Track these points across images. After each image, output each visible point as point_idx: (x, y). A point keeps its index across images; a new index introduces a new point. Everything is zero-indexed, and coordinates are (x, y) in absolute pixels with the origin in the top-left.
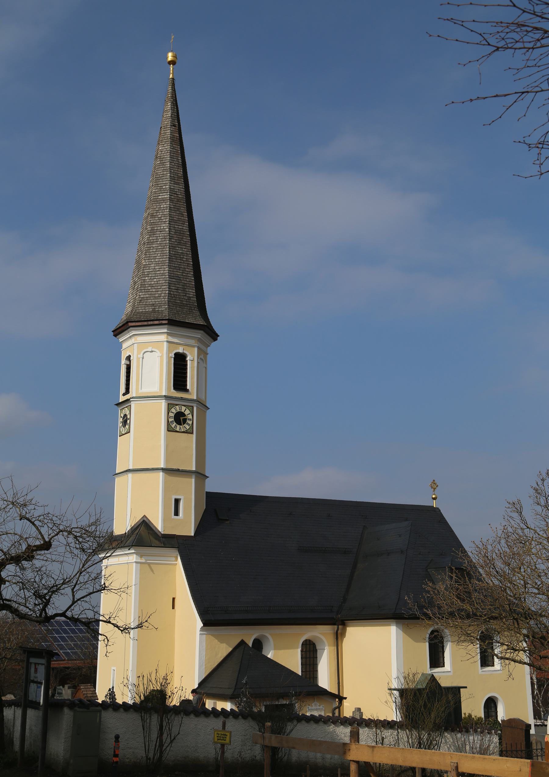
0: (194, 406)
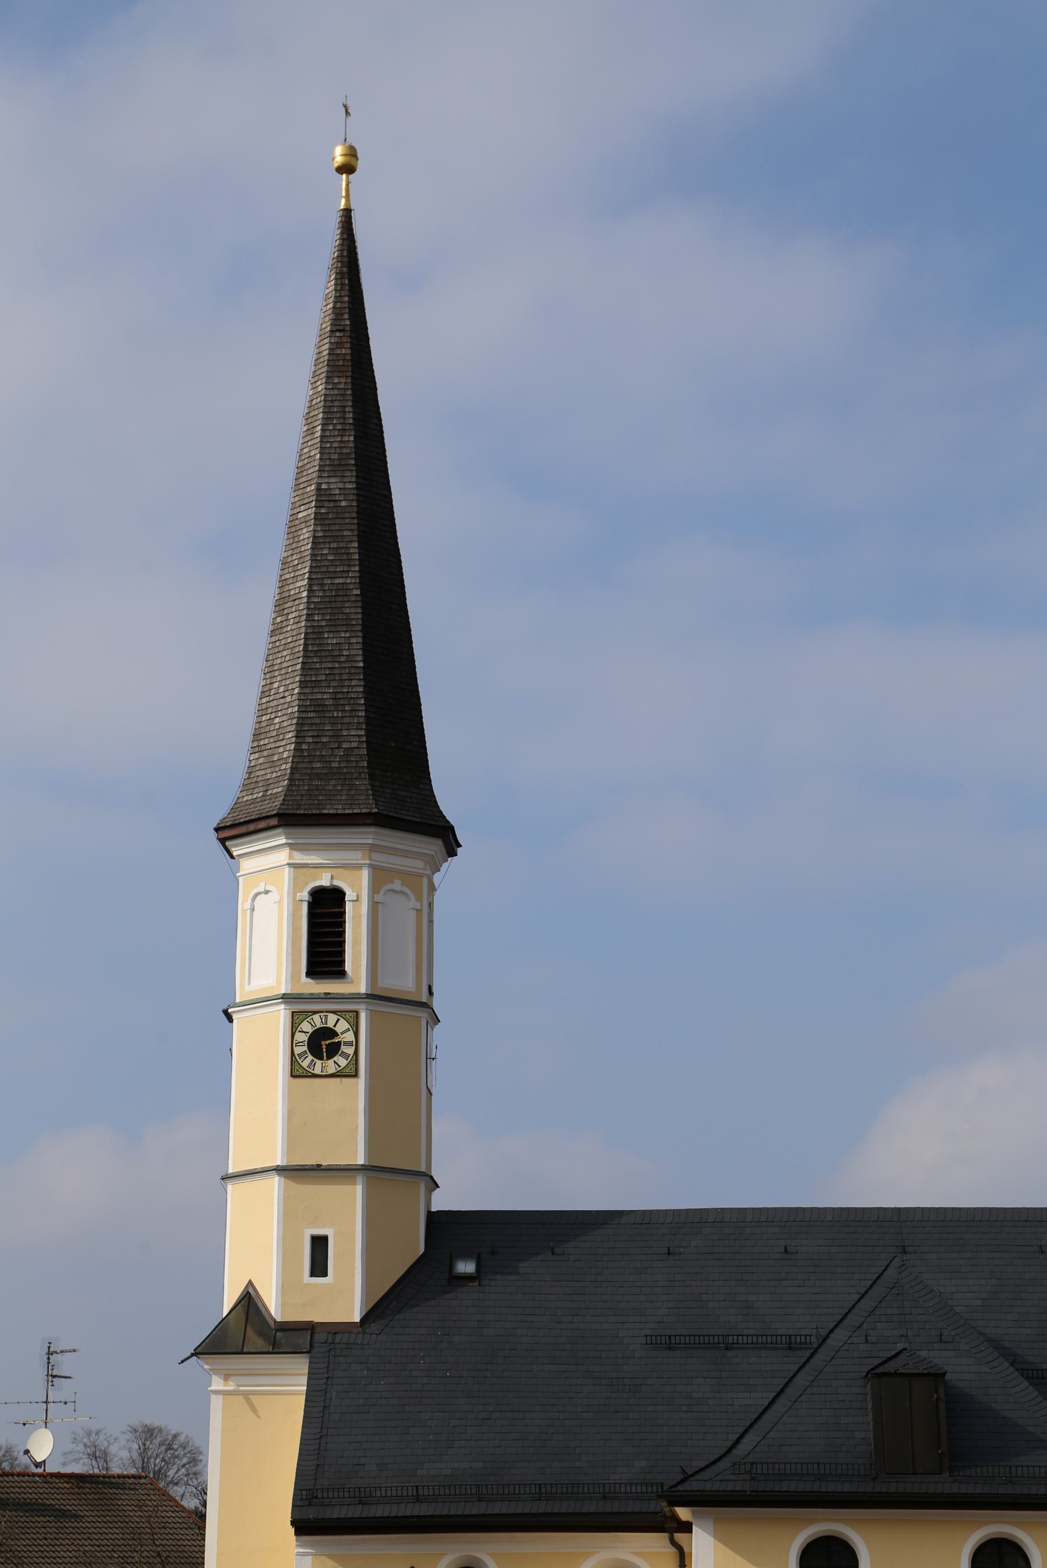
0: (361, 1011)
